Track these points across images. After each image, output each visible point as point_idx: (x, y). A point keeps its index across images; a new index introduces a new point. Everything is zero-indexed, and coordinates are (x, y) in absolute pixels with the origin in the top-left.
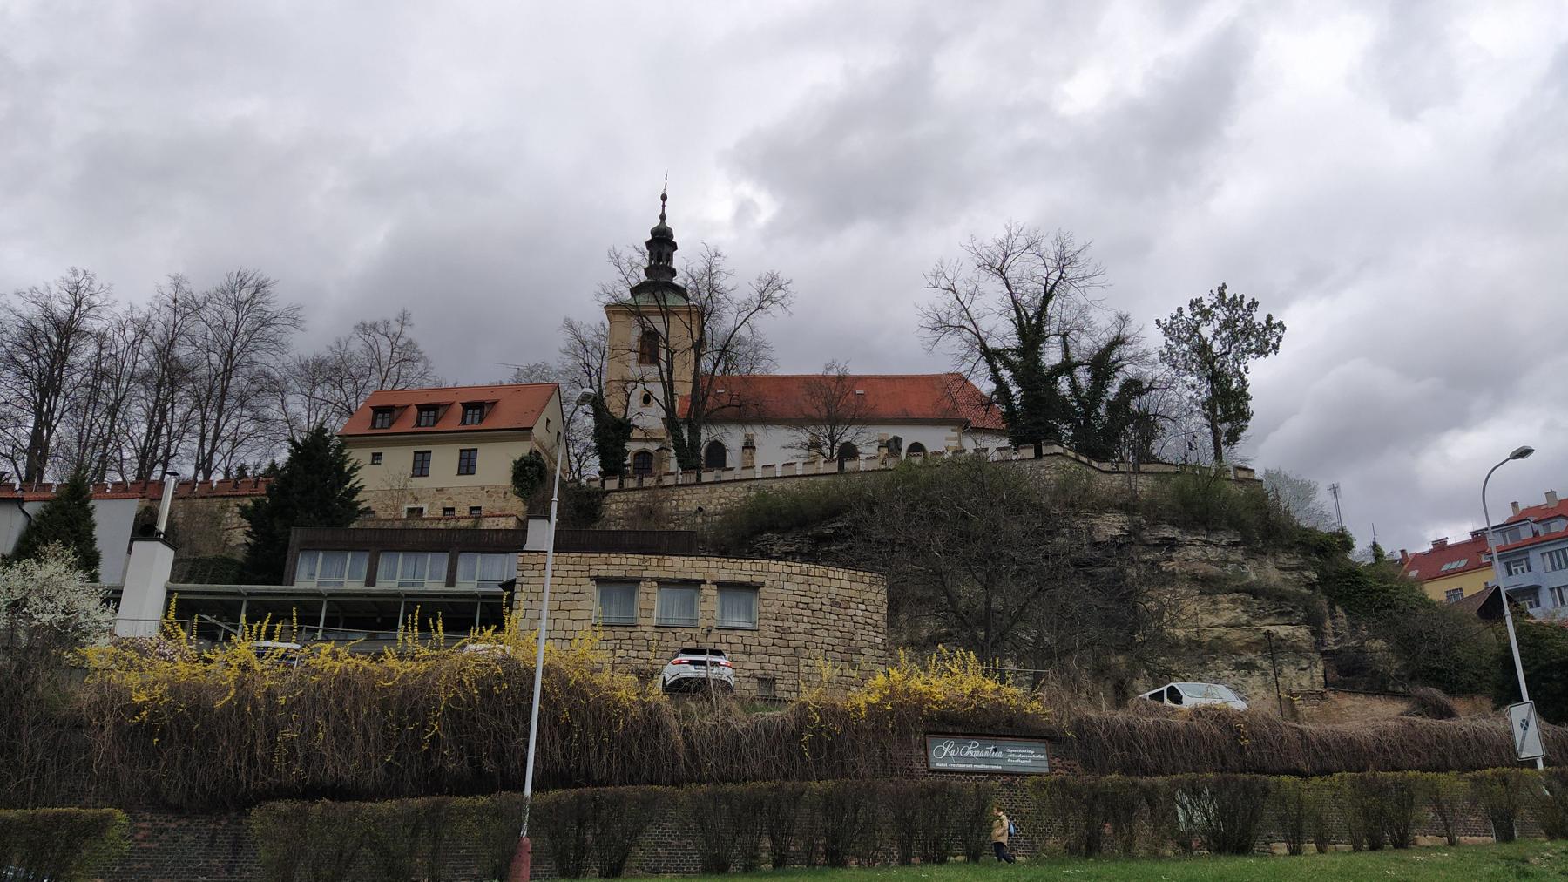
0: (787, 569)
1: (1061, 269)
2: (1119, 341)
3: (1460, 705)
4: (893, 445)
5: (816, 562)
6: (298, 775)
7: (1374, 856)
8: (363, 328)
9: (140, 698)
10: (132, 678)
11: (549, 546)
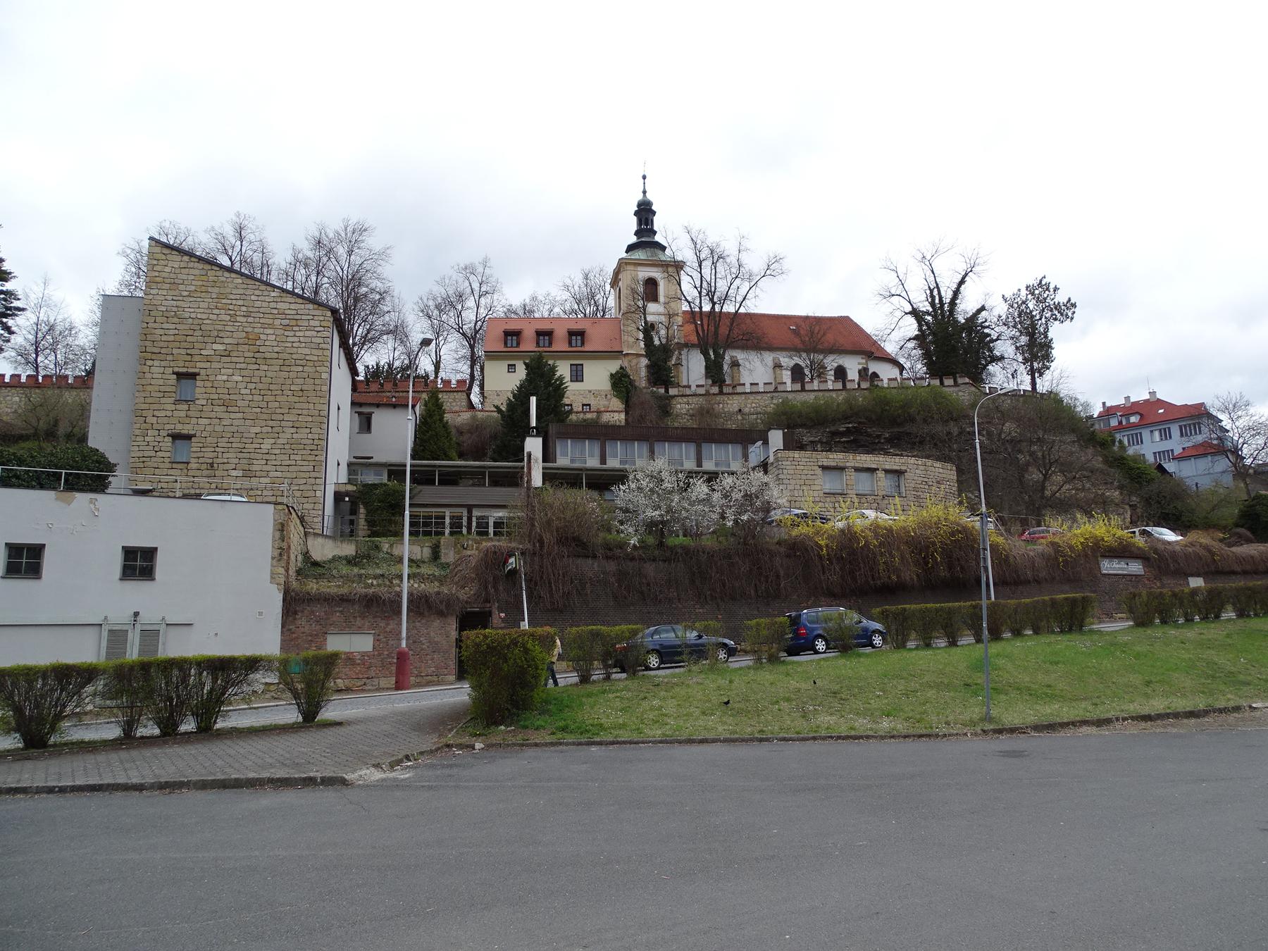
2: (983, 308)
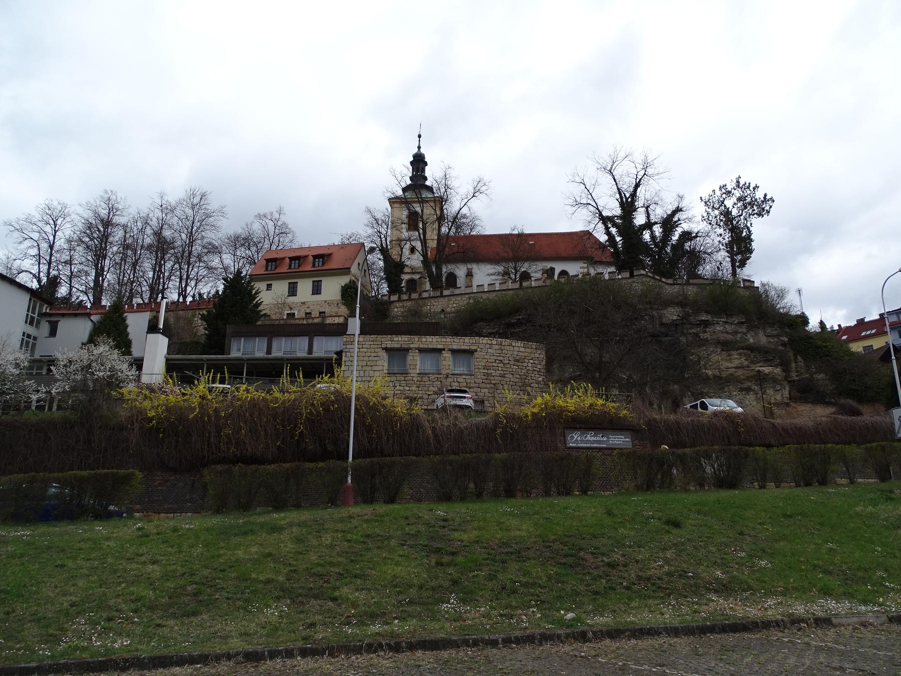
0: (489, 342)
1: (645, 169)
2: (678, 210)
3: (866, 409)
4: (550, 272)
5: (507, 338)
6: (233, 452)
7: (807, 490)
8: (259, 216)
9: (152, 414)
10: (147, 404)
11: (358, 332)
